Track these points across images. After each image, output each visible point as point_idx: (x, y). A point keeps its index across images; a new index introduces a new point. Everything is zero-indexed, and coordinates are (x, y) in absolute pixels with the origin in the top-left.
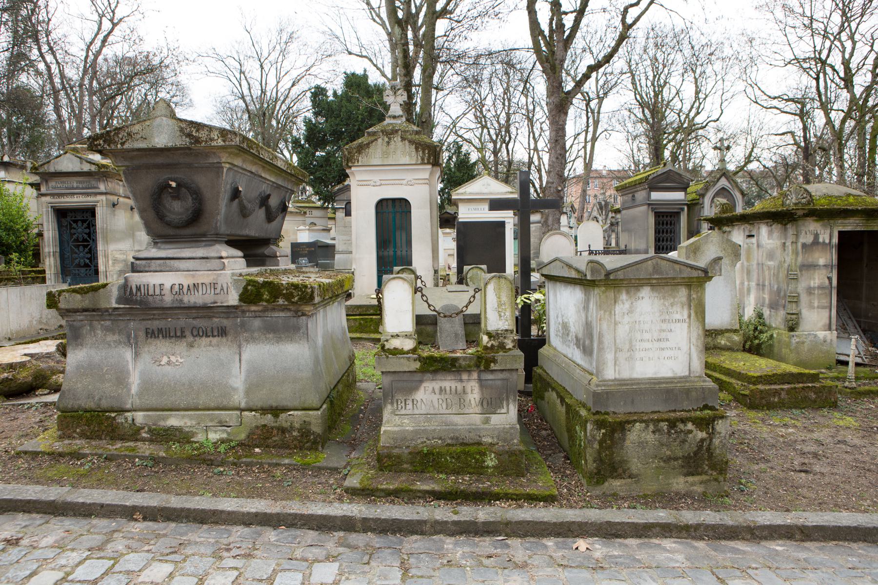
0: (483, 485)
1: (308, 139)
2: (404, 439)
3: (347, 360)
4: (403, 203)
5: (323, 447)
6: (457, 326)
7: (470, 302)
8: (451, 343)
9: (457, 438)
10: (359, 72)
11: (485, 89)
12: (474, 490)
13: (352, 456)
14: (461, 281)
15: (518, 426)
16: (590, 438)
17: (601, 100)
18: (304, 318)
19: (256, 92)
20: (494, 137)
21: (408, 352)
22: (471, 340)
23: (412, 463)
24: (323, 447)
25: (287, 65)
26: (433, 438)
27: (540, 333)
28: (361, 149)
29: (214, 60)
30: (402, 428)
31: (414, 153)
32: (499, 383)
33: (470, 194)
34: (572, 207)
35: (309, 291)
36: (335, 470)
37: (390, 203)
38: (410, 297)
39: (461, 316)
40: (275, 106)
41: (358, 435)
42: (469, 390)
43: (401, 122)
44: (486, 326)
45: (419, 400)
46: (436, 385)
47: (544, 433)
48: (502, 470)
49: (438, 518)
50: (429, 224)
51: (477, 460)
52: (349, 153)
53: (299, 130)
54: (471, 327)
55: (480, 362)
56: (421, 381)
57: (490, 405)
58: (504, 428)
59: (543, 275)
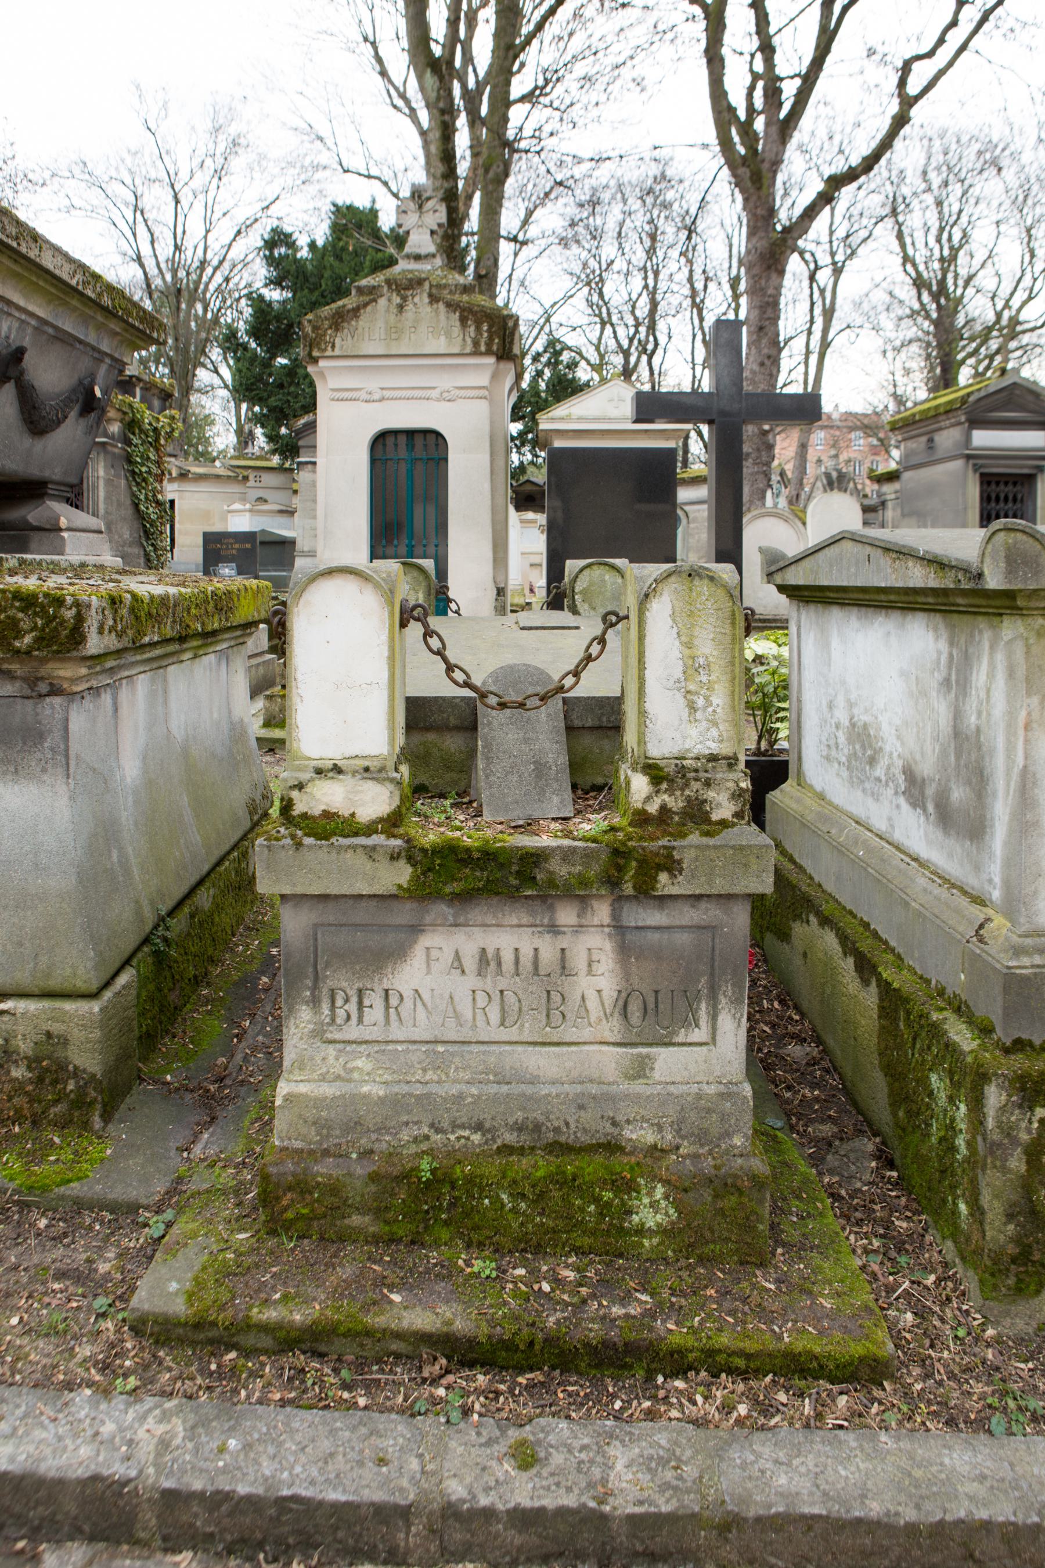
0: (624, 1311)
1: (255, 332)
2: (355, 1125)
3: (242, 813)
4: (431, 438)
5: (107, 1117)
6: (544, 738)
7: (589, 659)
8: (521, 803)
9: (537, 1127)
10: (362, 202)
11: (609, 250)
12: (594, 1331)
13: (197, 1151)
14: (556, 601)
15: (747, 1090)
16: (996, 1137)
17: (837, 271)
18: (57, 701)
19: (165, 250)
20: (625, 343)
21: (369, 829)
22: (591, 786)
23: (379, 1212)
24: (107, 1117)
25: (225, 198)
26: (455, 1126)
27: (764, 745)
28: (339, 320)
29: (83, 185)
30: (346, 1088)
31: (457, 330)
32: (683, 939)
33: (580, 419)
34: (782, 474)
35: (69, 614)
36: (125, 1213)
37: (402, 439)
38: (384, 637)
39: (556, 704)
40: (201, 277)
41: (239, 1057)
42: (579, 961)
43: (434, 267)
44: (642, 741)
45: (408, 994)
46: (469, 942)
47: (795, 1051)
48: (689, 1240)
49: (456, 1490)
50: (487, 486)
51: (604, 1208)
52: (315, 328)
53: (239, 317)
54: (587, 740)
55: (620, 869)
56: (416, 929)
57: (654, 1012)
58: (699, 1096)
59: (782, 589)
